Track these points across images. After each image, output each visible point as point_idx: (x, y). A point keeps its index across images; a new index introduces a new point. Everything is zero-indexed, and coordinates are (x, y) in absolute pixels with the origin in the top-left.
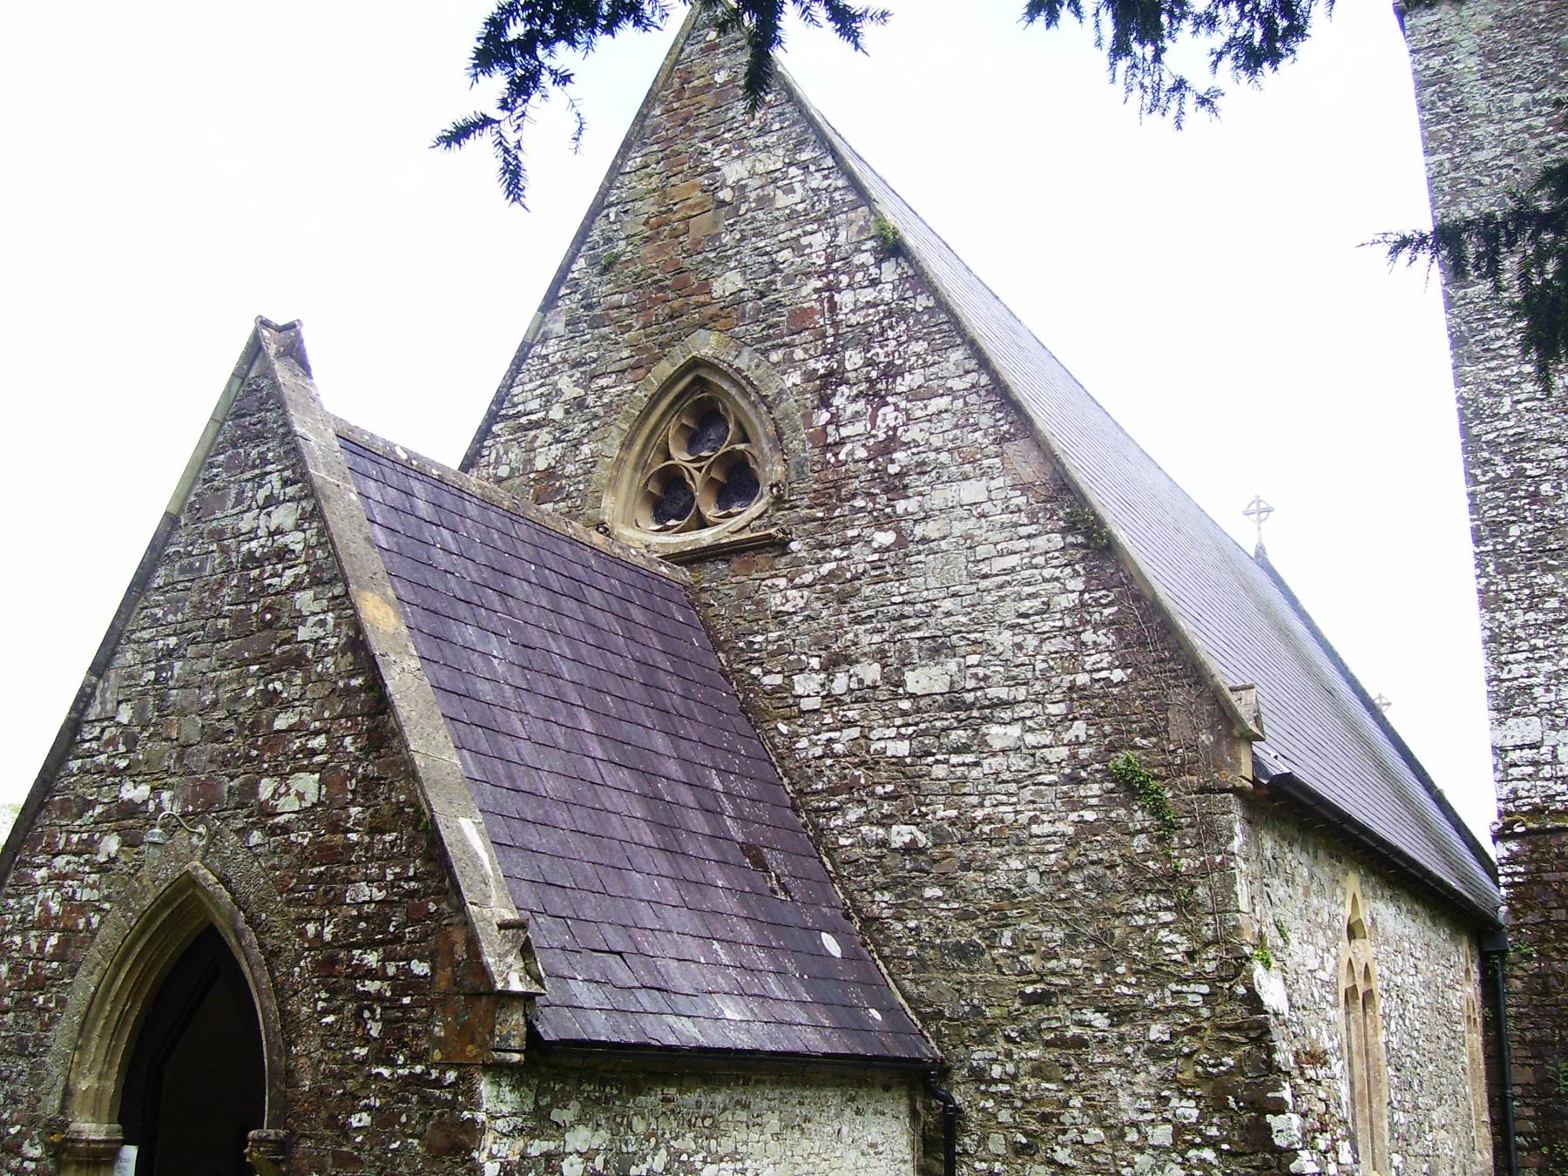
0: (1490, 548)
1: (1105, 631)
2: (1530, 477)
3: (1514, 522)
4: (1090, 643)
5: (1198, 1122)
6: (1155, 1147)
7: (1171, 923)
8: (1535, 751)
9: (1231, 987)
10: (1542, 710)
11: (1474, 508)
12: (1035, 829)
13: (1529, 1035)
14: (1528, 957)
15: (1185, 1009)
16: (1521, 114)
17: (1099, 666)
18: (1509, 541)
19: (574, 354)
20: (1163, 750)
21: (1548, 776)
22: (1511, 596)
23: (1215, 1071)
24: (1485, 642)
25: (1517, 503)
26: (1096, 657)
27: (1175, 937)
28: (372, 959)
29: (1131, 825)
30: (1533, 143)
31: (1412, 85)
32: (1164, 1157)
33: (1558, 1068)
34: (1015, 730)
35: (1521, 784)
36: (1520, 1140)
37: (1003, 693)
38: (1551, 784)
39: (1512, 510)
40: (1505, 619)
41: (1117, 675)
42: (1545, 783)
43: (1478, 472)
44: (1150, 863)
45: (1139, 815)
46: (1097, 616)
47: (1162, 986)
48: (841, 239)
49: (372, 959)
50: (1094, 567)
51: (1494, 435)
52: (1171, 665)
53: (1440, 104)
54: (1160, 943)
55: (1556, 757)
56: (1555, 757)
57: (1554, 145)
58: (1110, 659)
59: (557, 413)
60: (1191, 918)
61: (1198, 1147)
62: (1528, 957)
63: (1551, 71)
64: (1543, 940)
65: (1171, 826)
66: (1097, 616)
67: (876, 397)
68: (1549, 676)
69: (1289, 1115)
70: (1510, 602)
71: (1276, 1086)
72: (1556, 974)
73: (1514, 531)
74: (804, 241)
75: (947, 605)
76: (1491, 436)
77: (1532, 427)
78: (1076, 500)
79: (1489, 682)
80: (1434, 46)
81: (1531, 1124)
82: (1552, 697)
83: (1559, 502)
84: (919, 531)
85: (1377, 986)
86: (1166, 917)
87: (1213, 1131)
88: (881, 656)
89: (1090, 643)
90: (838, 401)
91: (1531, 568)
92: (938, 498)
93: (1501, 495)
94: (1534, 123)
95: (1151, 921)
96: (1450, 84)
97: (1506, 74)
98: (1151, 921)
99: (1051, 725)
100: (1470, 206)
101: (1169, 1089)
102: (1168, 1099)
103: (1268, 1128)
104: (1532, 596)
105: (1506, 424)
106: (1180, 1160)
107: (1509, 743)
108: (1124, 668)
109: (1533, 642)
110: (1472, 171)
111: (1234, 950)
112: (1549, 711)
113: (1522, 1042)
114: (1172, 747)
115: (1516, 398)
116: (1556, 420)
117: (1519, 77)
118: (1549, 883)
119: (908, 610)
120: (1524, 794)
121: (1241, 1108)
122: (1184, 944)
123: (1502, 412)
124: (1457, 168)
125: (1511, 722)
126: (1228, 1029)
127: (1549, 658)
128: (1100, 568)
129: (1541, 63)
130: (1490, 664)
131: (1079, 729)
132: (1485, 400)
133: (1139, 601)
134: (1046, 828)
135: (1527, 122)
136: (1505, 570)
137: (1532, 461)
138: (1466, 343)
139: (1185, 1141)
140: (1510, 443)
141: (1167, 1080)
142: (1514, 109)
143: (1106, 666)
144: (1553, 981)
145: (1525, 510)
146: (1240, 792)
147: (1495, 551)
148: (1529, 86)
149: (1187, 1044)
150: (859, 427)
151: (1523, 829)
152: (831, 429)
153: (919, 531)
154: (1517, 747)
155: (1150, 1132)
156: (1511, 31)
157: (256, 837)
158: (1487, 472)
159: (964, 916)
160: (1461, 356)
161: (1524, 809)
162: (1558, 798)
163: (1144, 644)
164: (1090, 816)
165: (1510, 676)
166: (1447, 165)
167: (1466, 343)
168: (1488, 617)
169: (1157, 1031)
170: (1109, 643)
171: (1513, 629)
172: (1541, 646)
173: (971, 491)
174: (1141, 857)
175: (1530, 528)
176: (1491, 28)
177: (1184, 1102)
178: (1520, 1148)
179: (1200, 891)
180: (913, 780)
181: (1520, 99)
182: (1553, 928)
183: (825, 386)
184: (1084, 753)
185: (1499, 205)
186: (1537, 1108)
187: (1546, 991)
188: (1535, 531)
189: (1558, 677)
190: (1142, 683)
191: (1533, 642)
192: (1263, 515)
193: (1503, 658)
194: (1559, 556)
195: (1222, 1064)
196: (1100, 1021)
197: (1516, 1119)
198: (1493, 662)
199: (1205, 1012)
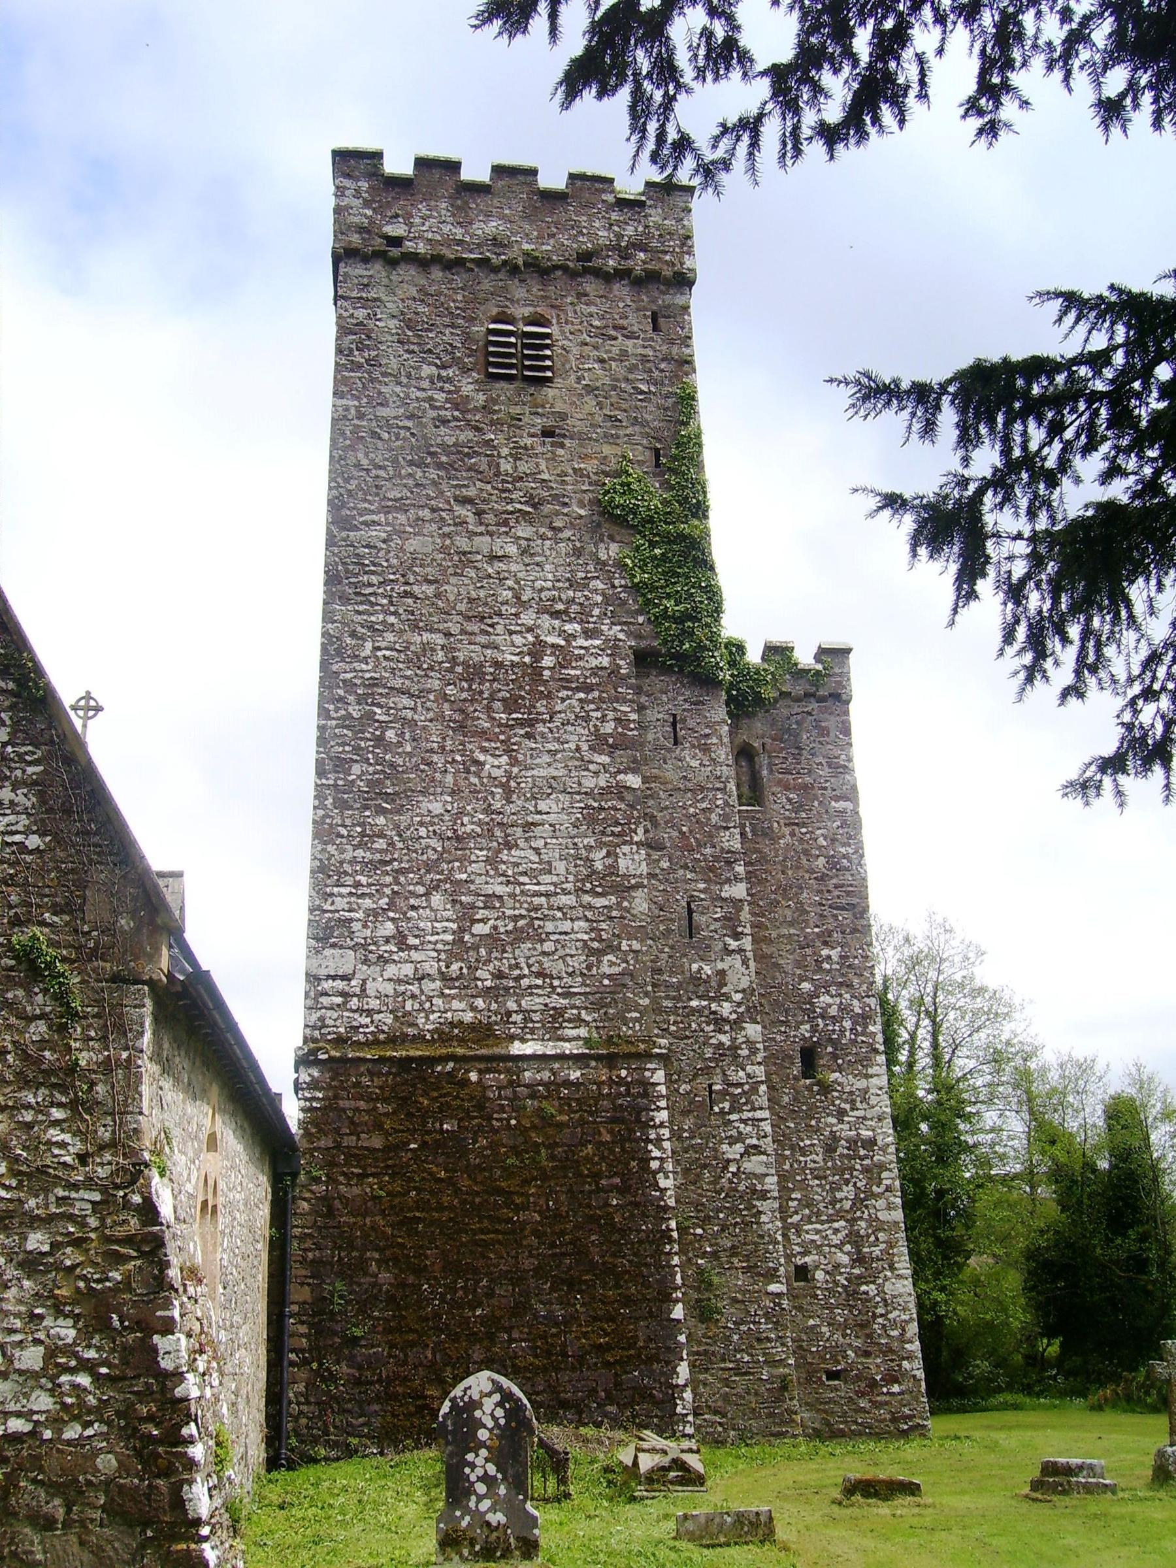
0: (331, 782)
1: (25, 791)
2: (378, 721)
3: (356, 761)
4: (6, 802)
5: (75, 1344)
6: (20, 1372)
7: (64, 1121)
8: (345, 983)
9: (126, 1195)
10: (357, 944)
11: (322, 741)
13: (310, 1255)
14: (317, 1180)
15: (71, 1218)
16: (425, 384)
17: (14, 828)
18: (351, 778)
20: (76, 931)
21: (354, 1008)
22: (344, 832)
23: (99, 1286)
24: (313, 872)
25: (363, 744)
26: (12, 818)
27: (67, 1137)
29: (29, 1008)
30: (434, 414)
31: (334, 329)
32: (31, 1383)
33: (334, 1288)
35: (329, 1013)
36: (292, 1356)
38: (356, 1016)
39: (357, 749)
40: (336, 853)
41: (34, 841)
42: (351, 1015)
43: (331, 707)
44: (47, 1054)
45: (40, 998)
46: (18, 773)
47: (47, 1191)
50: (23, 718)
51: (352, 675)
52: (96, 839)
53: (356, 353)
54: (49, 1143)
55: (365, 990)
56: (363, 990)
57: (449, 421)
58: (27, 822)
60: (88, 1117)
61: (73, 1371)
62: (317, 1180)
63: (459, 355)
64: (332, 1164)
65: (74, 1015)
66: (18, 773)
68: (369, 912)
69: (178, 1335)
70: (342, 837)
71: (168, 1305)
72: (341, 1197)
73: (356, 769)
76: (349, 676)
77: (387, 675)
78: (12, 641)
79: (311, 911)
80: (361, 298)
81: (304, 1340)
82: (368, 933)
83: (400, 750)
85: (221, 1200)
86: (57, 1114)
87: (91, 1354)
89: (6, 802)
91: (366, 807)
93: (350, 734)
94: (435, 396)
95: (40, 1117)
96: (369, 338)
97: (419, 344)
98: (40, 1117)
100: (367, 455)
101: (43, 1306)
102: (41, 1317)
103: (155, 1350)
104: (363, 834)
105: (364, 667)
106: (50, 1386)
107: (323, 972)
108: (42, 834)
109: (358, 878)
110: (374, 424)
111: (133, 1153)
112: (364, 946)
113: (303, 1261)
114: (86, 928)
115: (377, 644)
116: (409, 673)
117: (430, 351)
118: (344, 1110)
120: (331, 1022)
121: (125, 1328)
122: (77, 1146)
123: (363, 655)
124: (360, 416)
125: (328, 952)
126: (119, 1241)
127: (371, 895)
128: (31, 722)
129: (451, 345)
130: (314, 894)
132: (349, 640)
133: (69, 765)
135: (430, 393)
136: (342, 805)
137: (382, 707)
138: (340, 583)
139: (58, 1365)
140: (365, 686)
141: (41, 1296)
142: (421, 378)
143: (21, 829)
144: (337, 1204)
145: (369, 752)
146: (151, 983)
147: (336, 786)
148: (438, 361)
149: (70, 1256)
151: (326, 1056)
154: (329, 977)
155: (17, 1355)
156: (431, 308)
158: (340, 709)
160: (333, 594)
161: (329, 1037)
162: (361, 1030)
163: (68, 812)
165: (332, 908)
166: (353, 411)
167: (340, 583)
168: (319, 848)
169: (37, 1241)
170: (29, 804)
171: (341, 863)
172: (365, 883)
174: (38, 1045)
175: (371, 769)
176: (414, 299)
177: (60, 1322)
178: (292, 1364)
179: (100, 1088)
181: (427, 370)
182: (343, 1153)
185: (392, 462)
186: (311, 1326)
187: (331, 1213)
188: (375, 773)
189: (376, 915)
190: (60, 854)
191: (358, 878)
192: (91, 713)
193: (328, 890)
194: (393, 801)
195: (108, 1279)
197: (291, 1336)
198: (318, 893)
199: (93, 1222)
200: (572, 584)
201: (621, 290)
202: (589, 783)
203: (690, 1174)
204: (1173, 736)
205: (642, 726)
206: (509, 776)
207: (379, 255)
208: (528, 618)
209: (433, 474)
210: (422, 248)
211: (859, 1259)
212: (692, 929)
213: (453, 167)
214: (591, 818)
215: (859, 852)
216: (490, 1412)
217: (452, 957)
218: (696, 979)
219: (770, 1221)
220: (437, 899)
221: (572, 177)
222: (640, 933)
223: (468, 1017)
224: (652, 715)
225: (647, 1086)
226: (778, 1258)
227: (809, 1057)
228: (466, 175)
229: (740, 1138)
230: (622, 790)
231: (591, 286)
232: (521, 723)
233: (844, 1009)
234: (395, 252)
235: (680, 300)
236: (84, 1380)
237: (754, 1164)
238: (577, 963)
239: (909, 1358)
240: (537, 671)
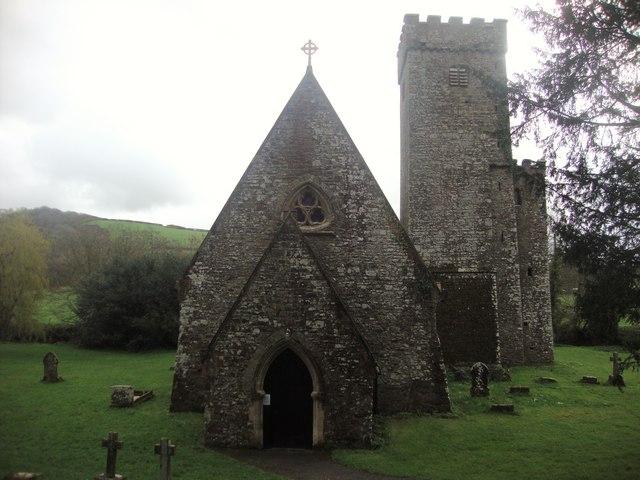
19: (268, 170)
28: (343, 359)
49: (343, 359)
59: (263, 186)
67: (359, 205)
88: (359, 266)
131: (405, 288)
150: (354, 211)
157: (306, 333)
169: (419, 348)
173: (383, 232)
183: (346, 198)
202: (478, 201)
203: (500, 302)
204: (609, 2)
205: (492, 186)
208: (462, 156)
212: (503, 240)
214: (479, 211)
216: (480, 370)
218: (503, 253)
223: (449, 262)
226: (521, 322)
229: (513, 292)
230: (485, 204)
233: (539, 259)
237: (515, 299)
238: (475, 248)
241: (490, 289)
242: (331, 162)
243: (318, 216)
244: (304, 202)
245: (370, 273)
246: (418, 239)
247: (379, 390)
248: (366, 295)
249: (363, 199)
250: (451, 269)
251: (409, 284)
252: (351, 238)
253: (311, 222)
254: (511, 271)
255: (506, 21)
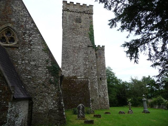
12: (42, 78)
34: (41, 69)
37: (40, 66)
39: (65, 53)
48: (27, 20)
67: (30, 36)
68: (66, 67)
74: (23, 18)
75: (35, 57)
84: (33, 50)
87: (56, 103)
88: (28, 60)
90: (25, 35)
92: (35, 47)
99: (45, 69)
119: (31, 56)
134: (44, 78)
136: (64, 58)
150: (28, 38)
152: (24, 38)
153: (33, 50)
159: (35, 85)
164: (47, 77)
169: (52, 95)
173: (39, 47)
180: (31, 72)
181: (71, 21)
183: (24, 33)
184: (47, 72)
196: (47, 94)
200: (83, 40)
201: (87, 15)
206: (77, 56)
207: (67, 11)
208: (79, 43)
209: (71, 30)
210: (70, 10)
211: (104, 95)
212: (92, 68)
213: (73, 3)
214: (84, 59)
215: (105, 62)
217: (73, 70)
218: (92, 72)
219: (98, 92)
220: (72, 66)
221: (83, 4)
222: (88, 69)
223: (74, 75)
224: (89, 51)
225: (88, 81)
227: (101, 79)
228: (74, 4)
229: (95, 85)
230: (86, 57)
231: (84, 14)
232: (78, 51)
233: (103, 75)
234: (68, 11)
235: (91, 16)
236: (56, 105)
237: (96, 87)
239: (108, 103)
240: (80, 47)
241: (88, 83)
242: (19, 20)
243: (12, 40)
244: (6, 34)
245: (32, 63)
246: (64, 67)
247: (33, 115)
248: (30, 72)
249: (31, 34)
250: (75, 77)
251: (48, 68)
252: (25, 49)
253: (9, 42)
254: (94, 78)
255: (93, 6)
